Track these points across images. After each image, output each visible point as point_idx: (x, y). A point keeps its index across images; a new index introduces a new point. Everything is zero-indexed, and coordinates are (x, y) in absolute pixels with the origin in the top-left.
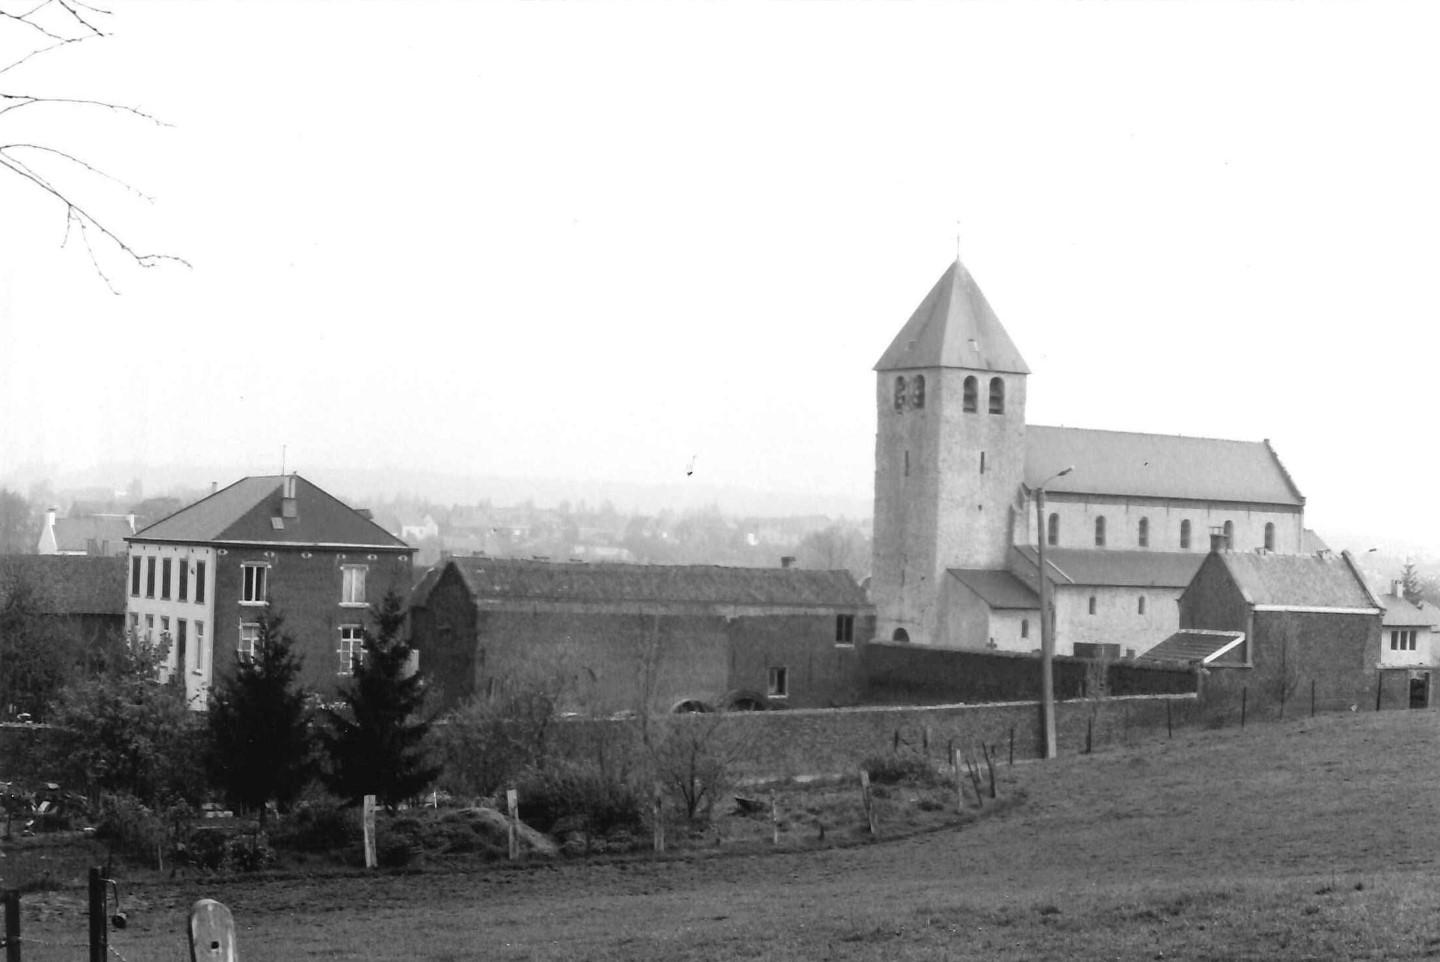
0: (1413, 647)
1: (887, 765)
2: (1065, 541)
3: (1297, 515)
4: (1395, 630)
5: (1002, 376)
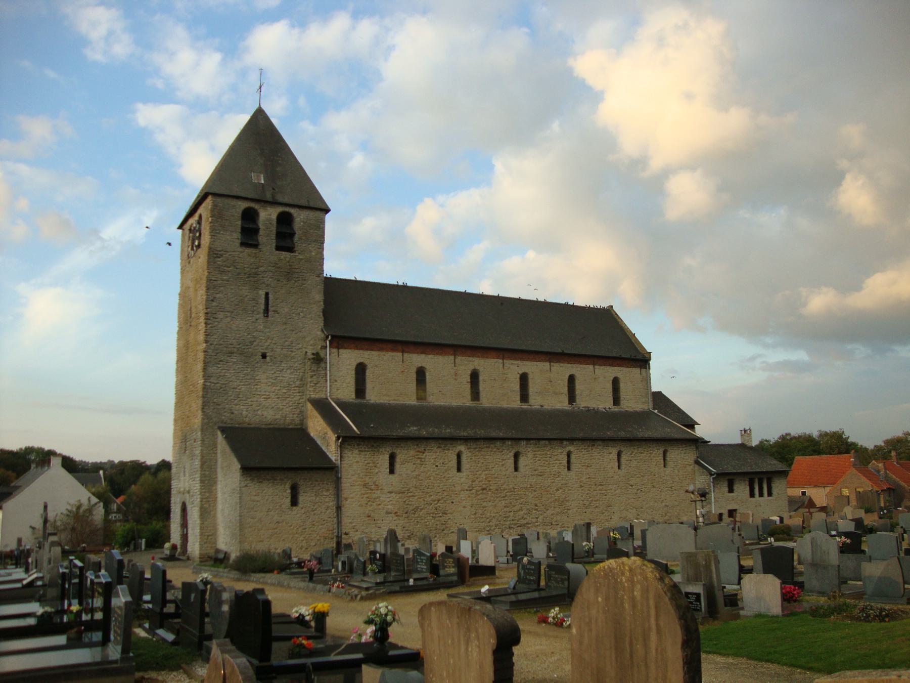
0: (770, 494)
1: (444, 612)
2: (536, 401)
3: (644, 371)
4: (730, 477)
5: (292, 211)
